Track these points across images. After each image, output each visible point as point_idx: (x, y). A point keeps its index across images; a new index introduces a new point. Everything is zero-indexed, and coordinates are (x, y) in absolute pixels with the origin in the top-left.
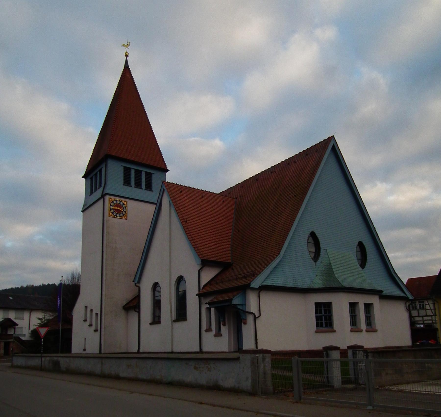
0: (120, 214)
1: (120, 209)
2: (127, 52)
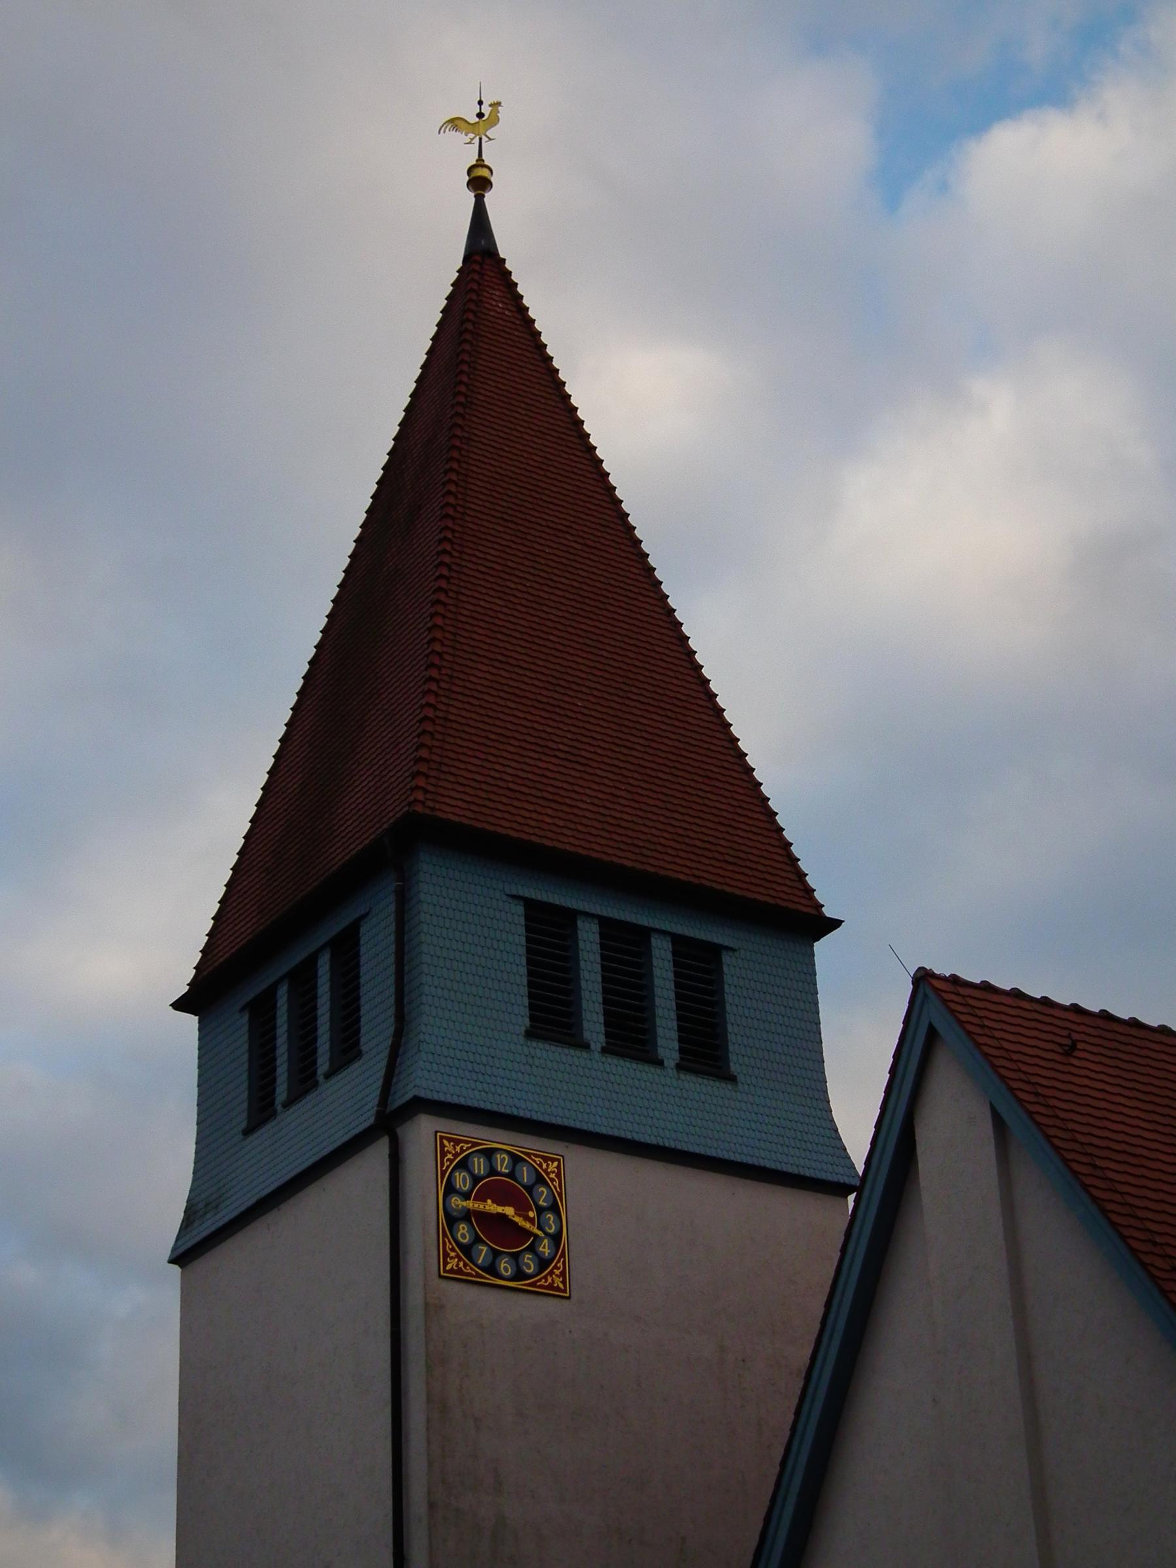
0: (516, 1257)
1: (517, 1219)
2: (480, 163)
